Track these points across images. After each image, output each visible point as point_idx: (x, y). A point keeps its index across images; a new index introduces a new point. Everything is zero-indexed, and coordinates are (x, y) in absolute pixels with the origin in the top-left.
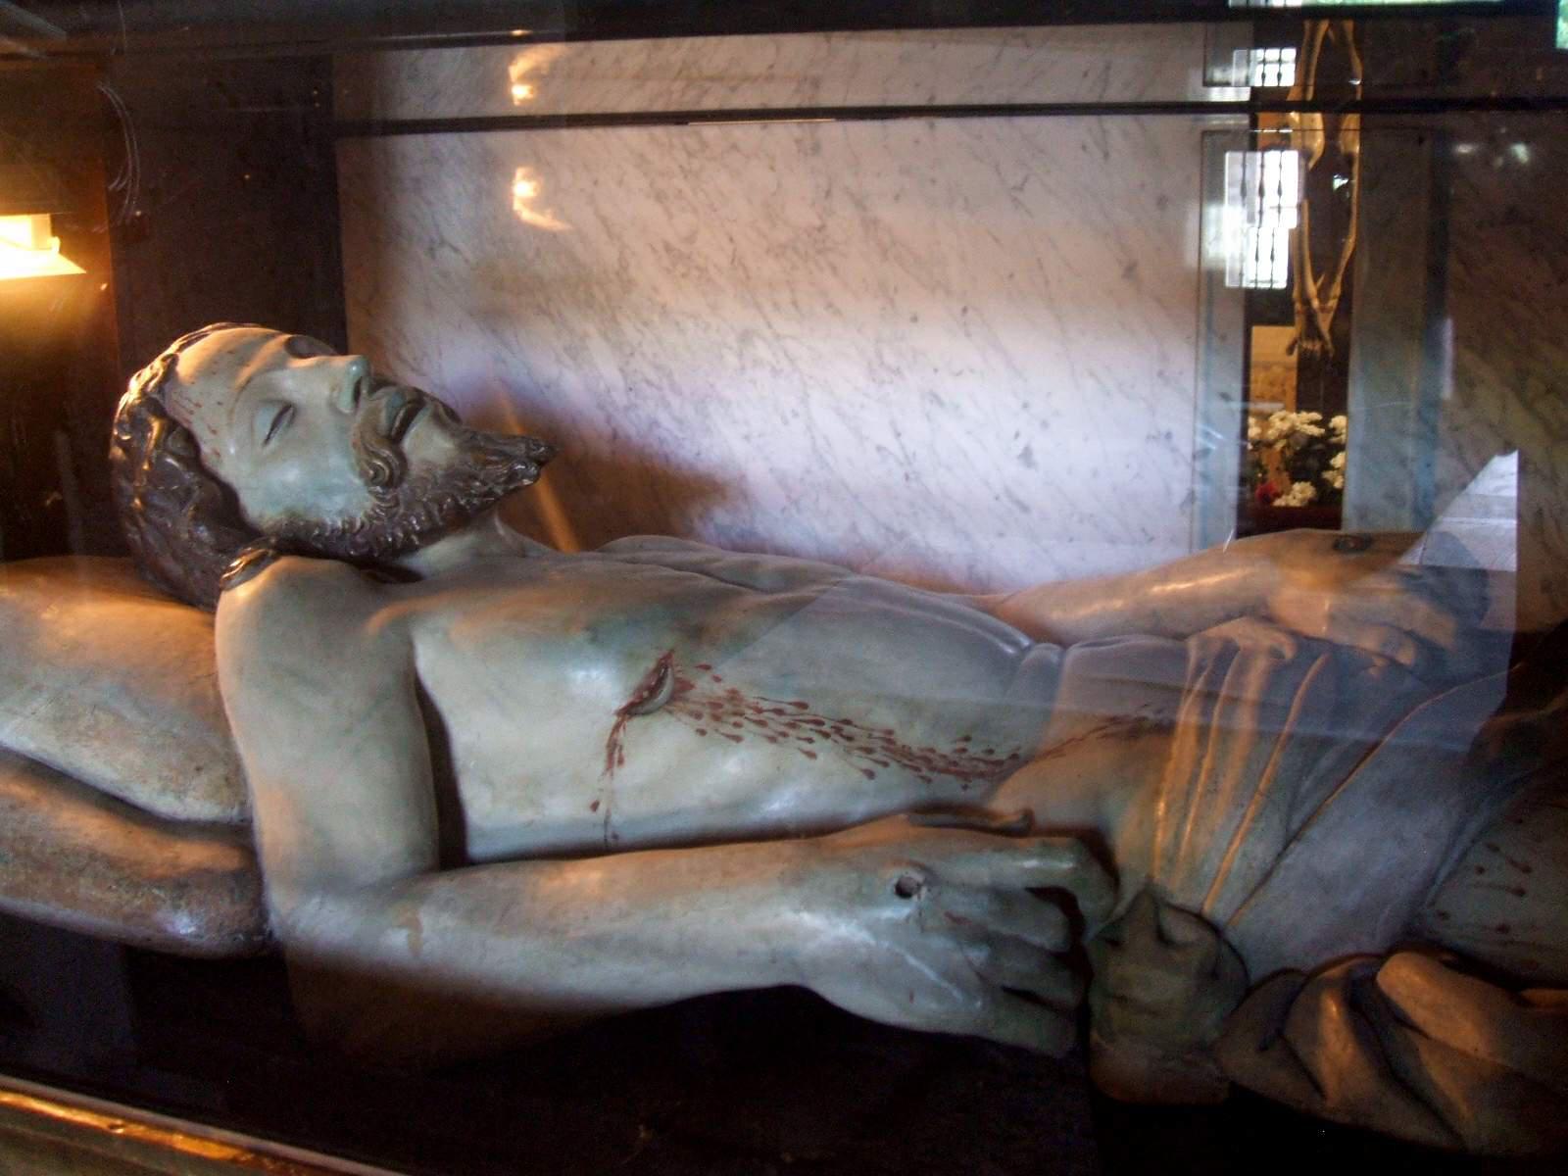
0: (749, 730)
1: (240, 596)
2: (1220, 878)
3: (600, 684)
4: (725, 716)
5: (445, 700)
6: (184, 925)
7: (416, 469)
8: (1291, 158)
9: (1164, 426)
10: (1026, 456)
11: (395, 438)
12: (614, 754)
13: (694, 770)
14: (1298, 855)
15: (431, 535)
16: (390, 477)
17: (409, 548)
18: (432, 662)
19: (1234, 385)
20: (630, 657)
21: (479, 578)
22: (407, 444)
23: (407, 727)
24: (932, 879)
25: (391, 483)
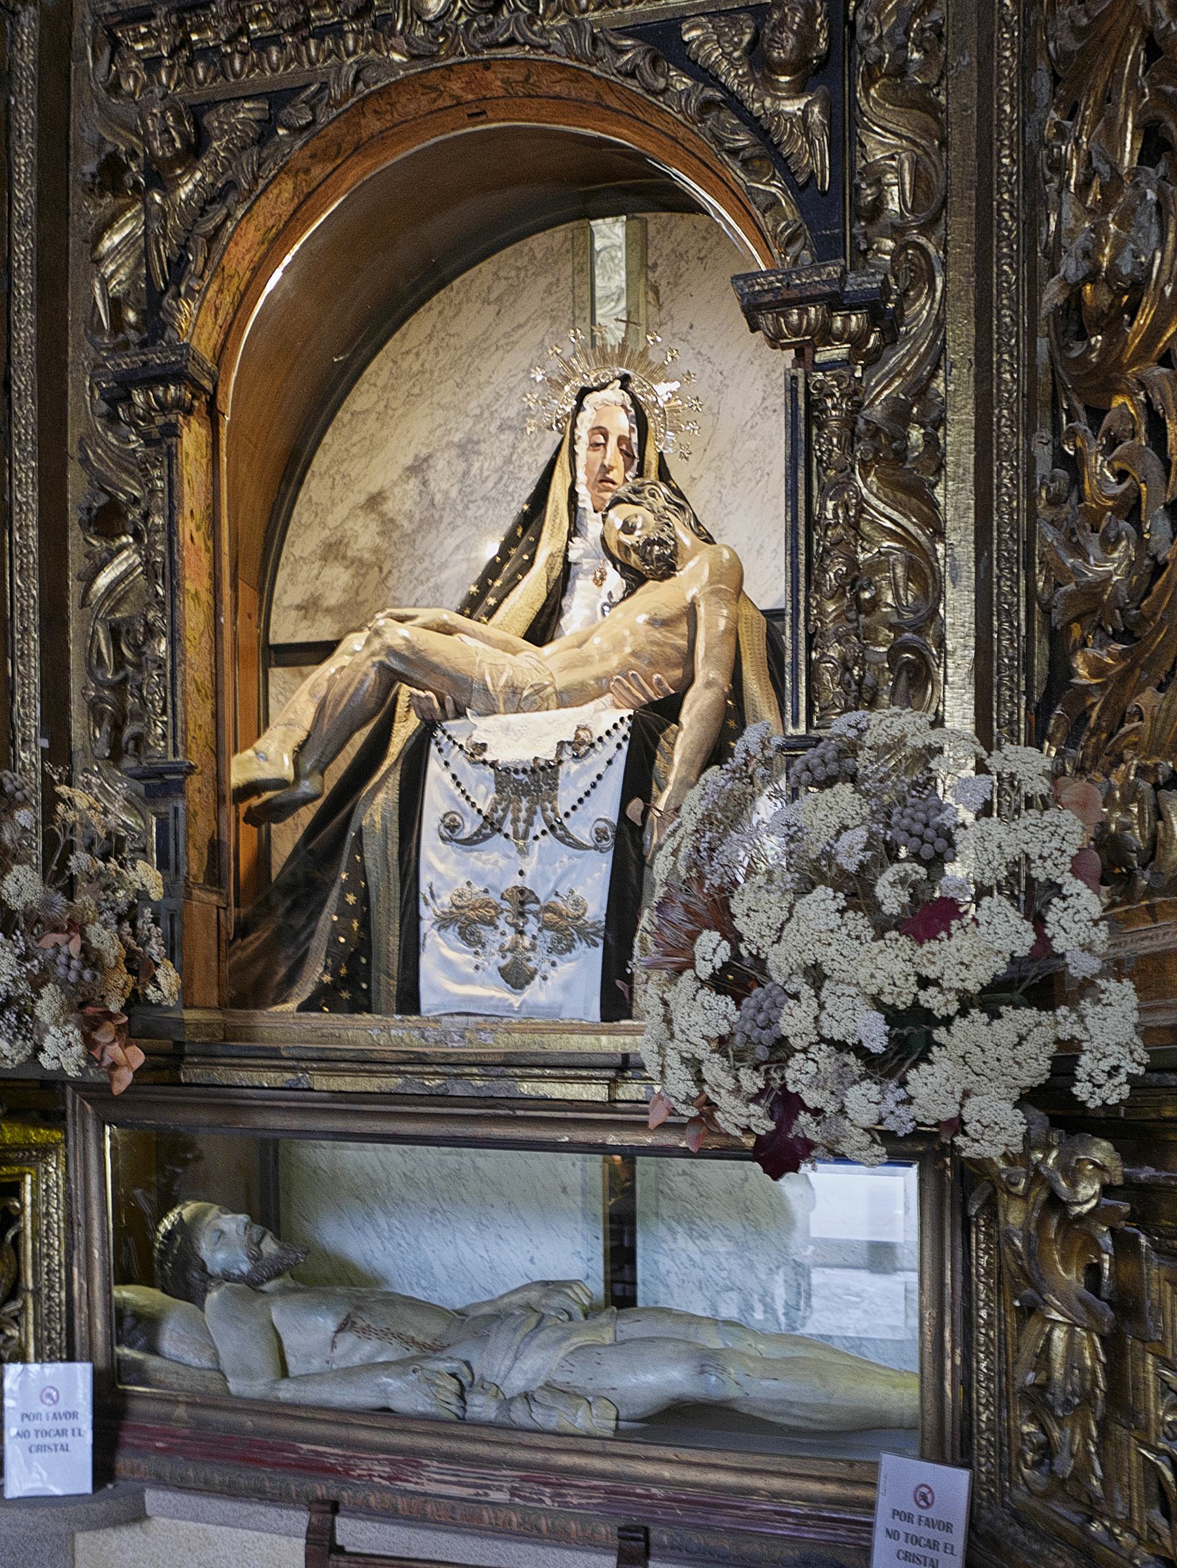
0: (373, 1337)
1: (213, 1296)
2: (698, 1539)
3: (329, 1324)
4: (366, 1332)
5: (280, 1330)
6: (212, 1387)
7: (265, 1255)
8: (88, 1367)
9: (579, 1249)
10: (532, 1260)
11: (258, 1244)
12: (333, 1345)
13: (358, 1349)
14: (518, 1364)
15: (269, 1279)
16: (256, 1258)
17: (262, 1283)
18: (275, 1316)
19: (220, 1256)
20: (337, 1314)
21: (284, 1291)
22: (262, 1246)
23: (271, 1335)
24: (422, 1368)
25: (257, 1260)
